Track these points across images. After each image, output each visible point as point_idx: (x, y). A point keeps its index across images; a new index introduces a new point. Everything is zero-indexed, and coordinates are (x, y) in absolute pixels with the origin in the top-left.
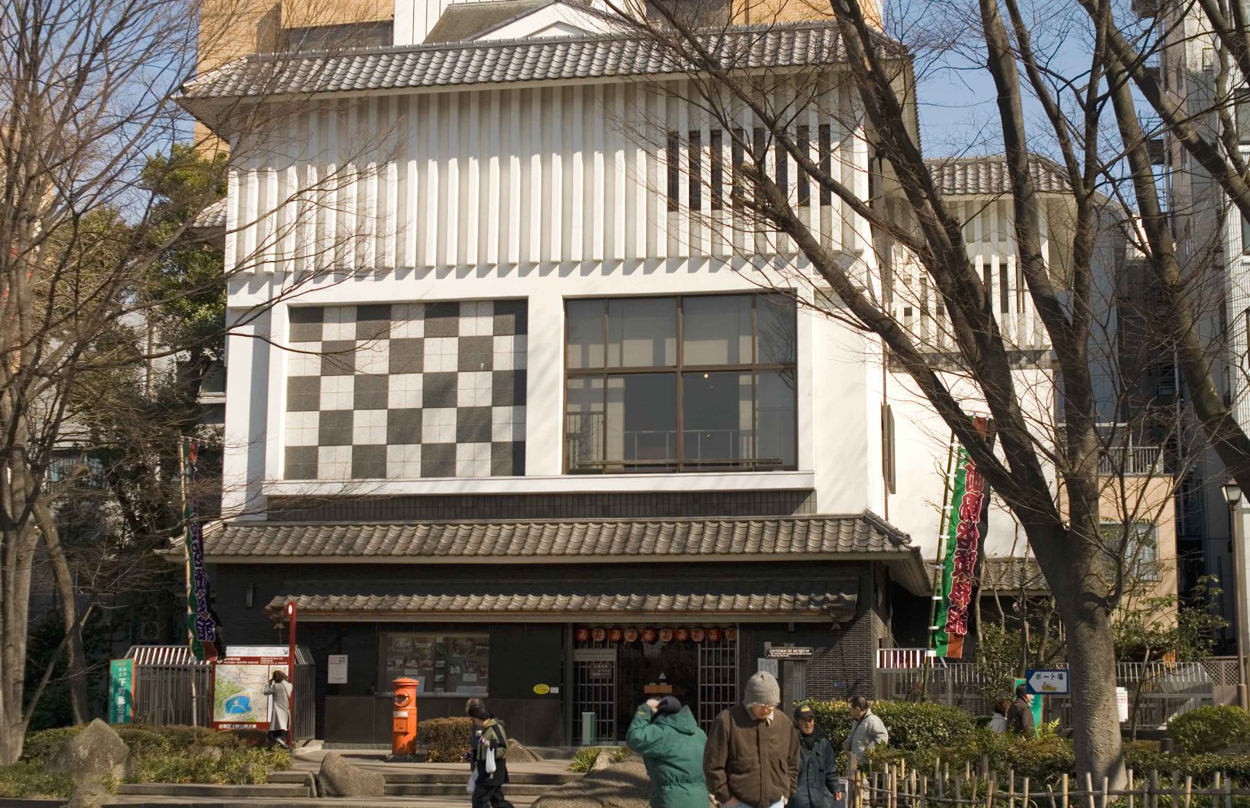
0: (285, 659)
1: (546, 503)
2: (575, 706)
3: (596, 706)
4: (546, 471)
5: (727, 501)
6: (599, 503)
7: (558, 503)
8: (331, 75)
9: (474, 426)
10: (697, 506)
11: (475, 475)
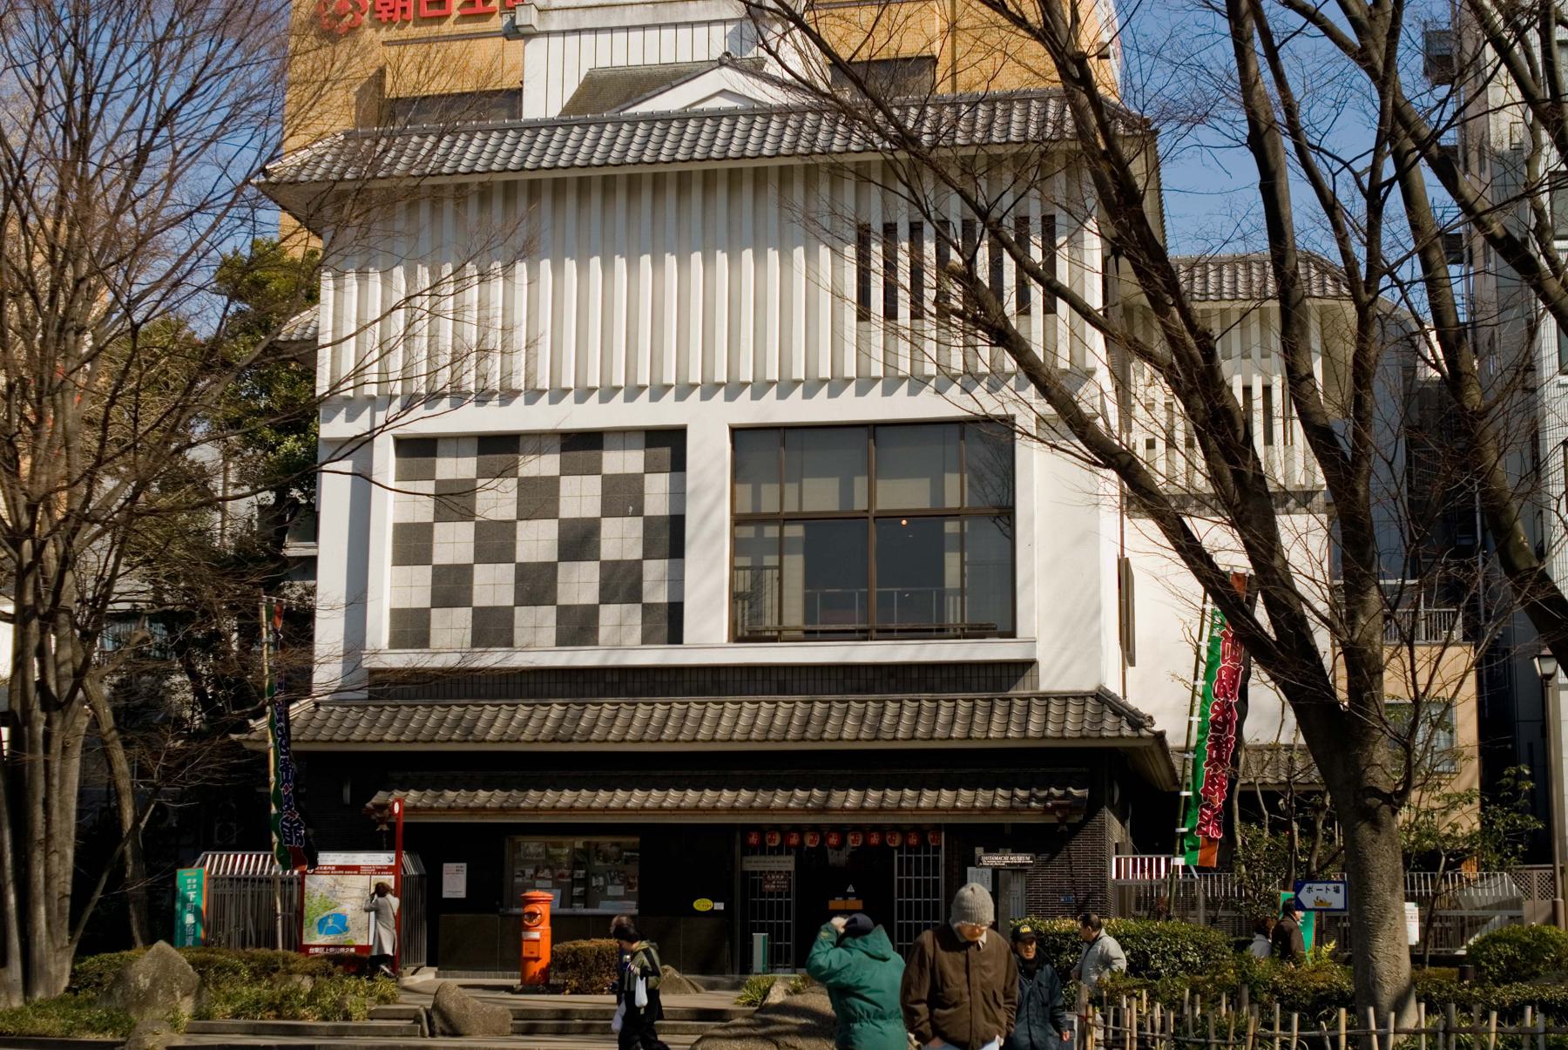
1: (708, 678)
4: (708, 638)
6: (774, 677)
7: (723, 677)
9: (621, 583)
11: (622, 643)
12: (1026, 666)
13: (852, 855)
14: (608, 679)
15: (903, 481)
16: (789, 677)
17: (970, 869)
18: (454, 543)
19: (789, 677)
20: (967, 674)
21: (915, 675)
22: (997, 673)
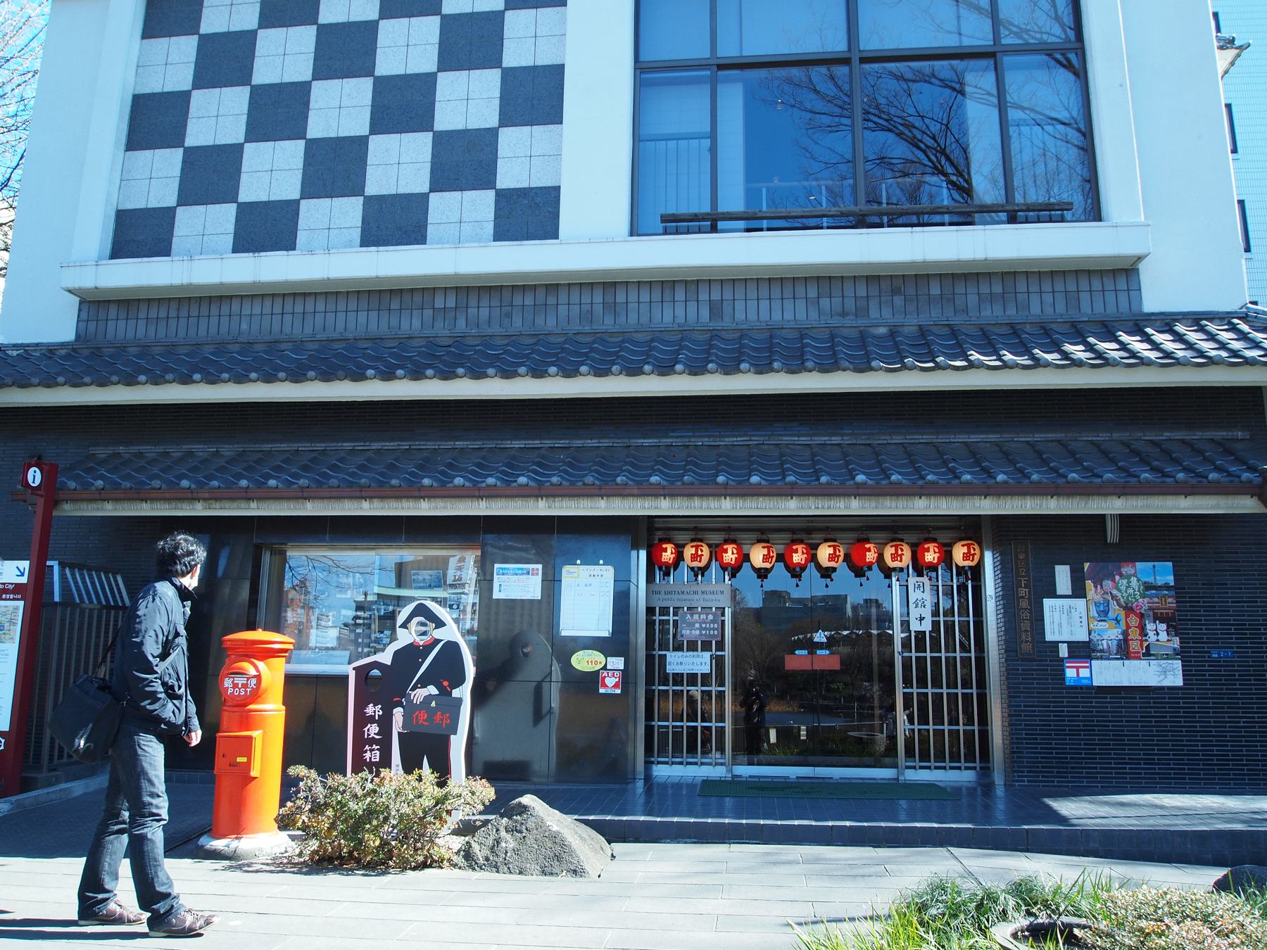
0: (18, 589)
1: (598, 298)
2: (646, 762)
3: (666, 683)
4: (597, 236)
5: (960, 289)
6: (704, 296)
7: (621, 298)
8: (497, 614)
9: (465, 160)
10: (898, 300)
11: (462, 246)
12: (1125, 272)
13: (397, 654)
14: (439, 303)
15: (258, 15)
16: (728, 295)
17: (1048, 603)
18: (467, 100)
19: (728, 295)
20: (1022, 287)
21: (935, 290)
22: (1072, 287)
